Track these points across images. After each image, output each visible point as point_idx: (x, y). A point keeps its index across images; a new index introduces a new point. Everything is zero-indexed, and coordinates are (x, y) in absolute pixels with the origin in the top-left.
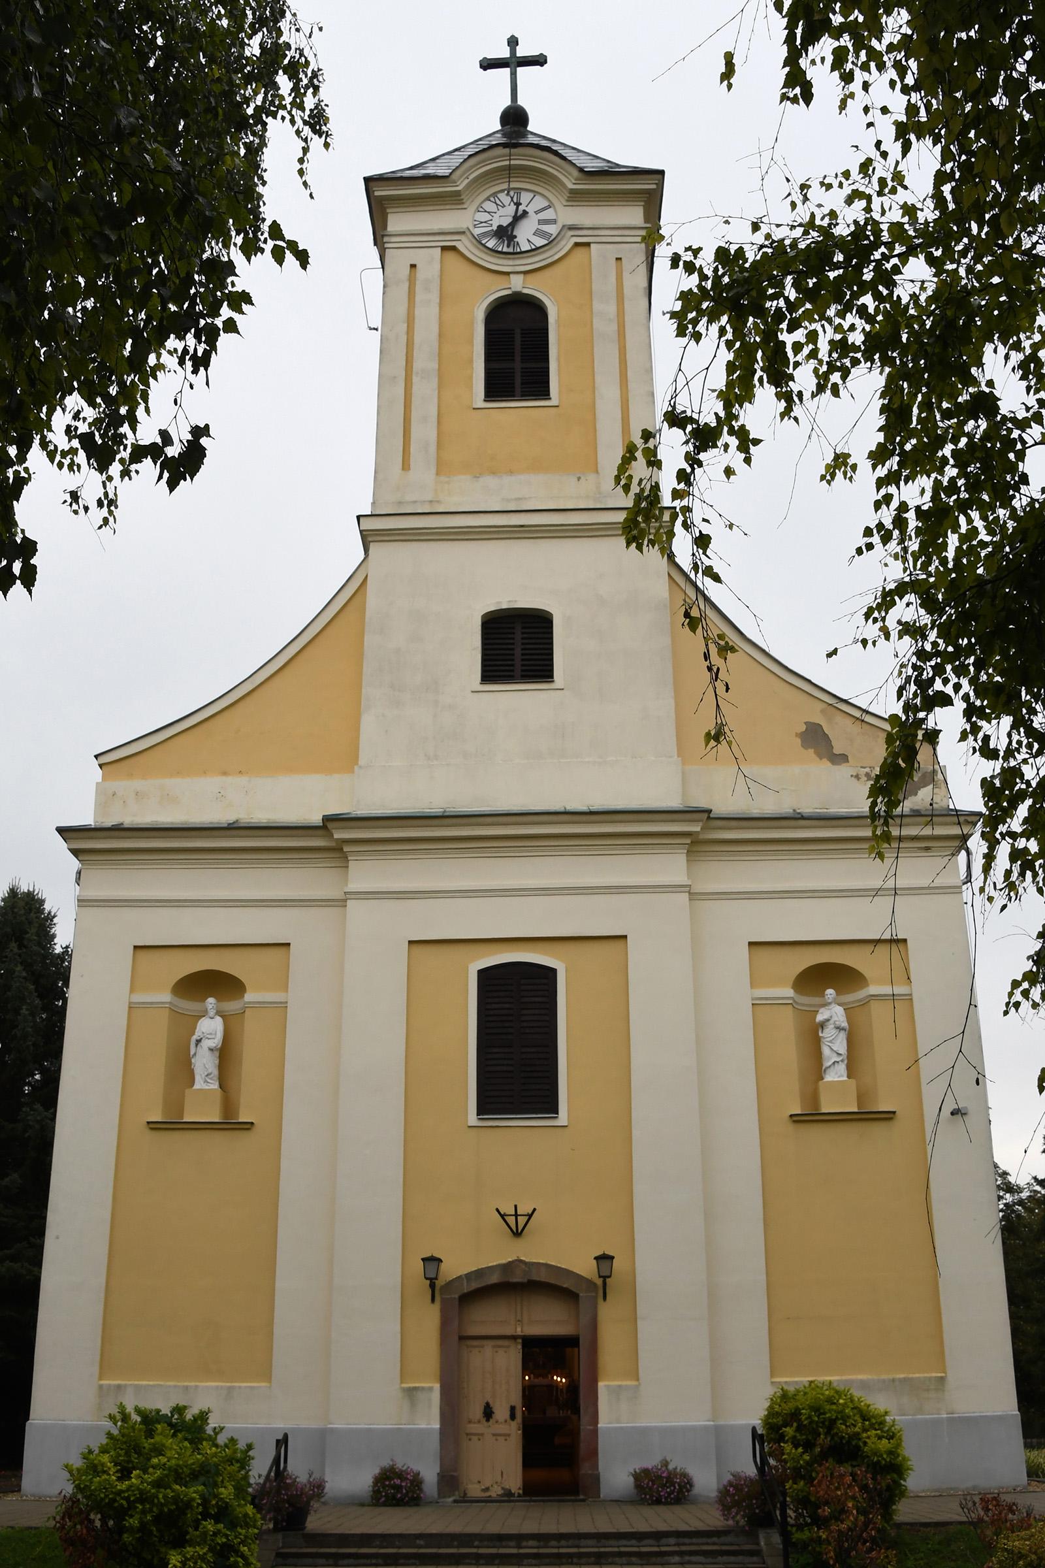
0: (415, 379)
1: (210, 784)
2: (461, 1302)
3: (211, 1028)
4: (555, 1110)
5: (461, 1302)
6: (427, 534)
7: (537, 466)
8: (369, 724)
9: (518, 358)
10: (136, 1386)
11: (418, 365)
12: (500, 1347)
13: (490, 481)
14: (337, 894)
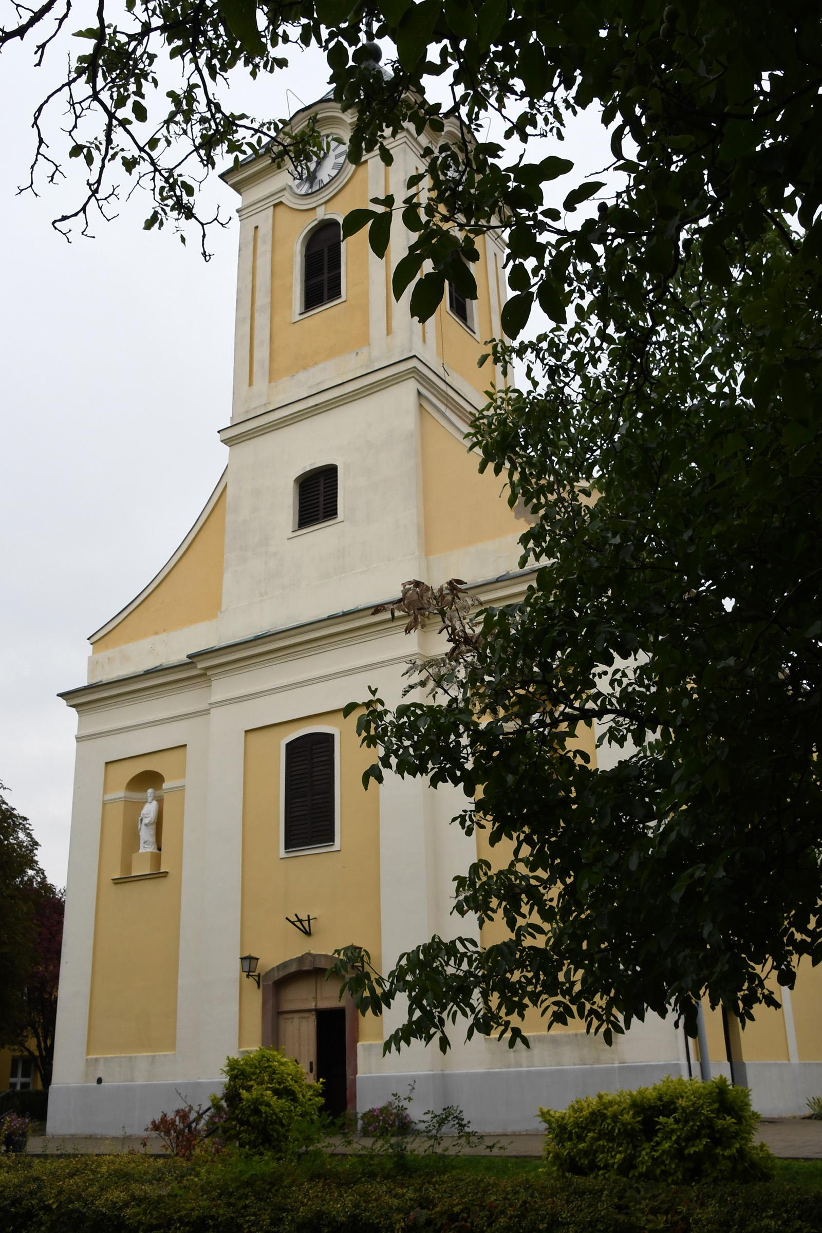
0: (256, 315)
1: (145, 644)
2: (277, 986)
3: (150, 810)
4: (332, 839)
5: (277, 986)
6: (285, 421)
7: (333, 352)
8: (228, 578)
9: (326, 271)
10: (106, 1059)
11: (258, 304)
12: (304, 1018)
13: (302, 376)
14: (204, 706)
